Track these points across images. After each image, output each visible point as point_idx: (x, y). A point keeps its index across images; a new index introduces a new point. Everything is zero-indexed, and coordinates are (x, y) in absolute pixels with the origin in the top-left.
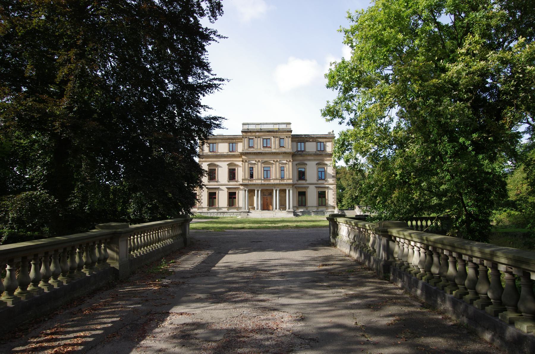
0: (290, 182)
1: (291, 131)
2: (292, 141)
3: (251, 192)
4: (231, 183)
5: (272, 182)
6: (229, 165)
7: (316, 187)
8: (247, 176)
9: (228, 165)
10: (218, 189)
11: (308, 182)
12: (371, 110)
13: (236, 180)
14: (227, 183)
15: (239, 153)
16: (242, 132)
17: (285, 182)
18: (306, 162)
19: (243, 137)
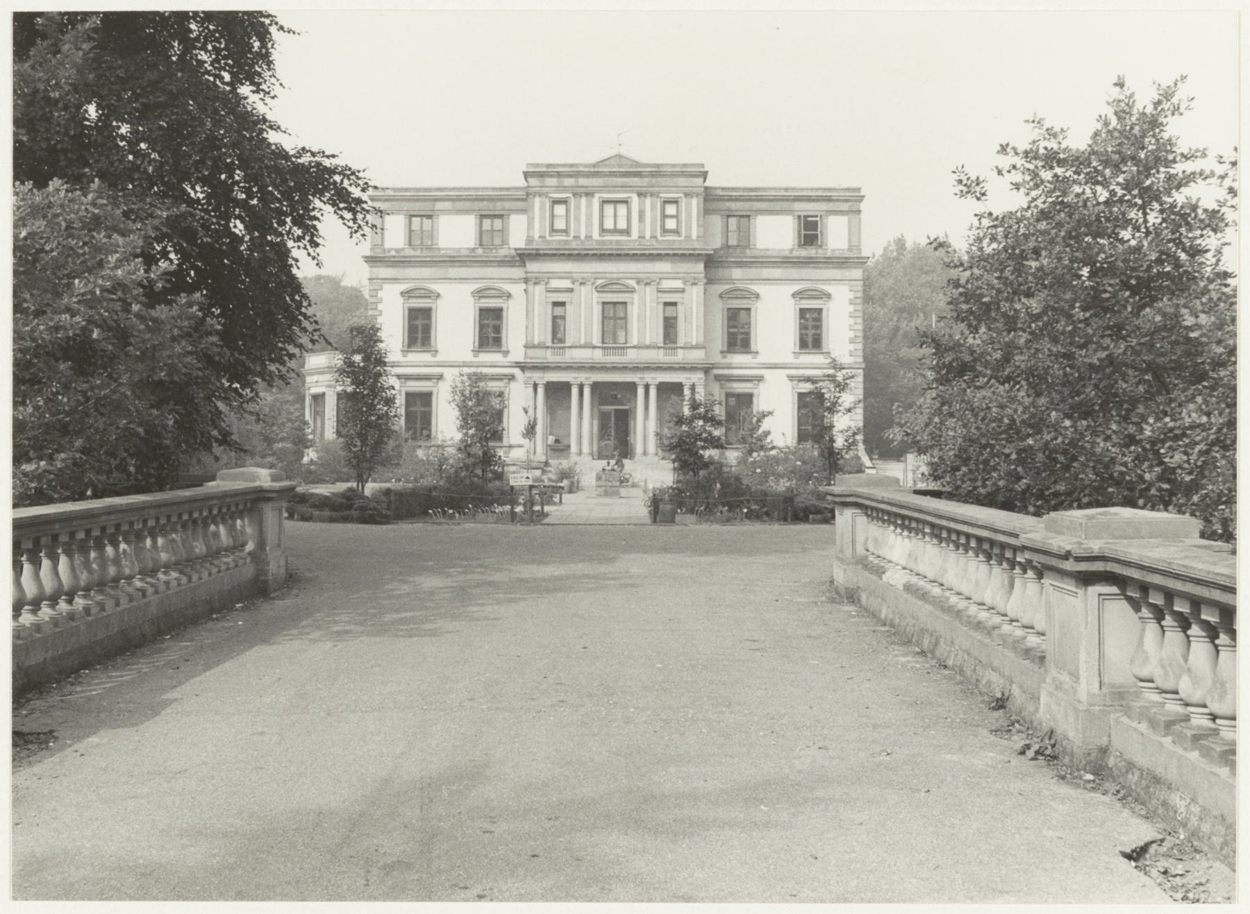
0: (697, 356)
1: (704, 175)
2: (707, 212)
3: (557, 393)
4: (413, 357)
5: (632, 356)
6: (479, 294)
7: (791, 378)
8: (542, 333)
9: (406, 294)
10: (760, 379)
11: (761, 359)
12: (107, 157)
13: (824, 350)
14: (790, 359)
15: (513, 252)
16: (527, 175)
17: (681, 356)
18: (755, 288)
19: (528, 194)
